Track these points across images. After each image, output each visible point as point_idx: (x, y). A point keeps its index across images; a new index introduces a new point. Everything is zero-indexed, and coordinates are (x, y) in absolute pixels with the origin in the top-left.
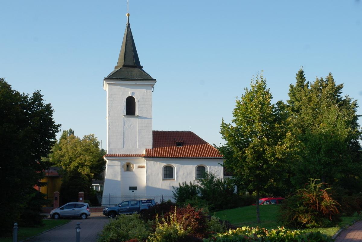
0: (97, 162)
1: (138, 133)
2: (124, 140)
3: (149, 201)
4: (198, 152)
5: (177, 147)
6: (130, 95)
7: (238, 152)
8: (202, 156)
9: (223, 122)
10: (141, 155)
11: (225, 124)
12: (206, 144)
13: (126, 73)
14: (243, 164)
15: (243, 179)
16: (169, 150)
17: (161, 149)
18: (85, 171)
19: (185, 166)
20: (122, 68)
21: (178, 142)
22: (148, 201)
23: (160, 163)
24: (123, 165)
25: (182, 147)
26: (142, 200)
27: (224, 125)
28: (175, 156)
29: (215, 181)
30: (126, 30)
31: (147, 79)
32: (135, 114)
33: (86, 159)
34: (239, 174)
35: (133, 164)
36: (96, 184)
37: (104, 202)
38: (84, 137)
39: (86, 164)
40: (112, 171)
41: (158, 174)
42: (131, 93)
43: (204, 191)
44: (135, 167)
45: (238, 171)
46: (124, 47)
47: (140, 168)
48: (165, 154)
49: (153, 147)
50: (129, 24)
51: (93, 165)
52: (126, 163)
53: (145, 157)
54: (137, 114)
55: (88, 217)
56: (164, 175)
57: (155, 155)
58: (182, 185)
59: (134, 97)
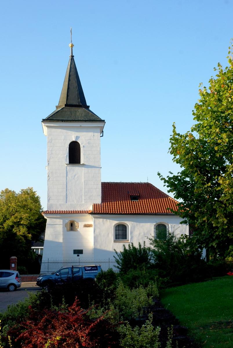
0: (36, 220)
1: (84, 184)
2: (66, 193)
3: (96, 268)
4: (157, 207)
5: (131, 201)
6: (74, 140)
7: (204, 184)
8: (162, 211)
9: (174, 131)
10: (87, 211)
11: (178, 135)
12: (167, 198)
13: (69, 113)
14: (214, 207)
15: (214, 237)
16: (121, 205)
17: (112, 204)
18: (21, 231)
19: (142, 224)
20: (64, 108)
21: (133, 195)
22: (93, 268)
23: (111, 220)
25: (138, 202)
26: (85, 267)
27: (177, 137)
28: (129, 211)
29: (174, 242)
30: (70, 64)
31: (94, 119)
32: (80, 163)
33: (22, 217)
34: (206, 226)
35: (77, 223)
36: (35, 246)
37: (43, 268)
38: (21, 191)
39: (22, 223)
40: (54, 231)
41: (108, 234)
42: (75, 137)
43: (159, 256)
44: (80, 226)
45: (205, 221)
46: (67, 83)
47: (87, 227)
48: (117, 209)
49: (102, 201)
50: (72, 56)
51: (31, 224)
52: (70, 221)
53: (92, 213)
54: (82, 162)
55: (17, 288)
56: (116, 235)
57: (104, 211)
58: (127, 248)
59: (78, 141)
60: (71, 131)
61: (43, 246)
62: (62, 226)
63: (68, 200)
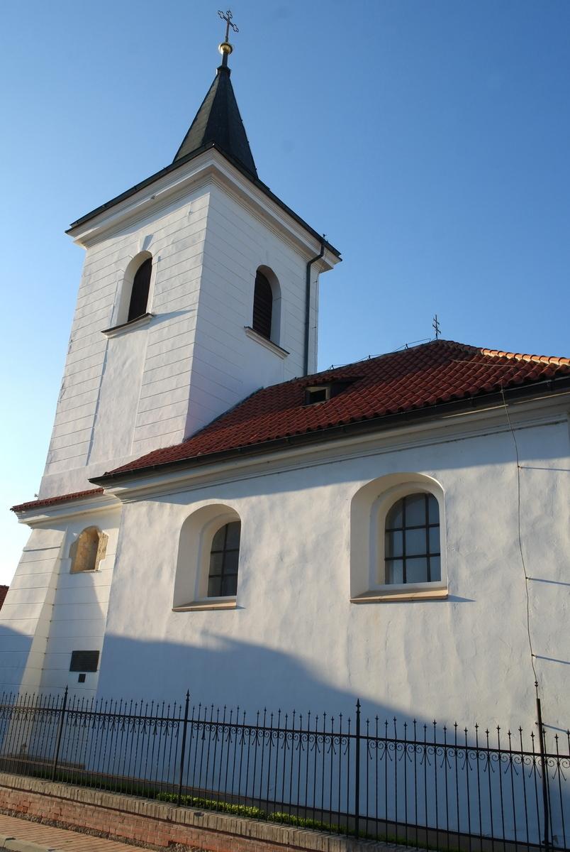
24: (72, 545)
41: (160, 569)
54: (149, 310)
62: (56, 553)
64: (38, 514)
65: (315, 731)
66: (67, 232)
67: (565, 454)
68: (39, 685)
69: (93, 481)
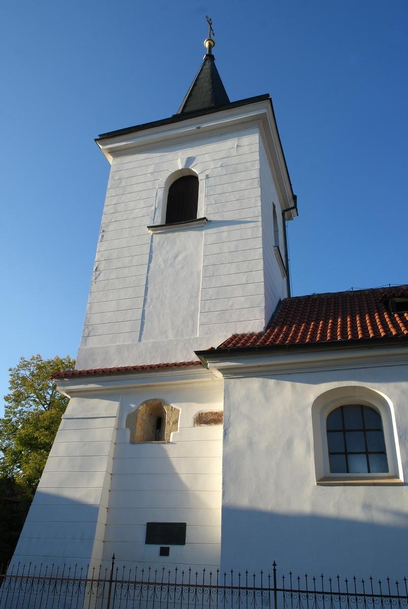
23: (298, 384)
24: (129, 416)
41: (289, 444)
44: (182, 414)
47: (208, 422)
52: (146, 402)
54: (201, 214)
60: (175, 151)
61: (161, 548)
62: (113, 423)
63: (144, 332)
64: (87, 383)
65: (397, 595)
66: (96, 140)
67: (405, 380)
68: (101, 559)
69: (198, 353)
